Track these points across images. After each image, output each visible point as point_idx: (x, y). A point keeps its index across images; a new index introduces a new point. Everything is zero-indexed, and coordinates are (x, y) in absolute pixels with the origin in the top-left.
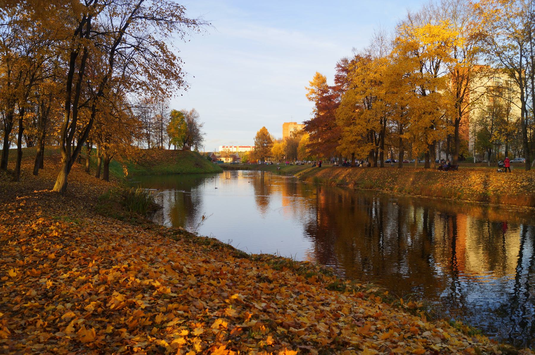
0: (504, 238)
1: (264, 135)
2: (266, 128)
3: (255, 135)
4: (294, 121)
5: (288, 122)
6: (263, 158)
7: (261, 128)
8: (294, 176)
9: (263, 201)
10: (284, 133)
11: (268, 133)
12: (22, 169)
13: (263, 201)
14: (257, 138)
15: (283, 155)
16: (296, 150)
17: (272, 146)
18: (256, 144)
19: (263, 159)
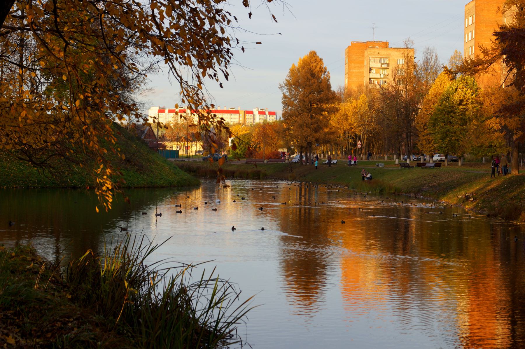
0: (513, 337)
1: (313, 75)
2: (320, 55)
3: (283, 75)
4: (383, 39)
5: (364, 38)
6: (310, 144)
7: (304, 54)
8: (444, 201)
9: (306, 274)
10: (349, 74)
11: (323, 70)
12: (18, 55)
13: (306, 274)
14: (289, 84)
15: (356, 137)
16: (410, 121)
17: (335, 111)
18: (287, 102)
19: (306, 147)
